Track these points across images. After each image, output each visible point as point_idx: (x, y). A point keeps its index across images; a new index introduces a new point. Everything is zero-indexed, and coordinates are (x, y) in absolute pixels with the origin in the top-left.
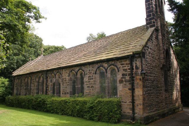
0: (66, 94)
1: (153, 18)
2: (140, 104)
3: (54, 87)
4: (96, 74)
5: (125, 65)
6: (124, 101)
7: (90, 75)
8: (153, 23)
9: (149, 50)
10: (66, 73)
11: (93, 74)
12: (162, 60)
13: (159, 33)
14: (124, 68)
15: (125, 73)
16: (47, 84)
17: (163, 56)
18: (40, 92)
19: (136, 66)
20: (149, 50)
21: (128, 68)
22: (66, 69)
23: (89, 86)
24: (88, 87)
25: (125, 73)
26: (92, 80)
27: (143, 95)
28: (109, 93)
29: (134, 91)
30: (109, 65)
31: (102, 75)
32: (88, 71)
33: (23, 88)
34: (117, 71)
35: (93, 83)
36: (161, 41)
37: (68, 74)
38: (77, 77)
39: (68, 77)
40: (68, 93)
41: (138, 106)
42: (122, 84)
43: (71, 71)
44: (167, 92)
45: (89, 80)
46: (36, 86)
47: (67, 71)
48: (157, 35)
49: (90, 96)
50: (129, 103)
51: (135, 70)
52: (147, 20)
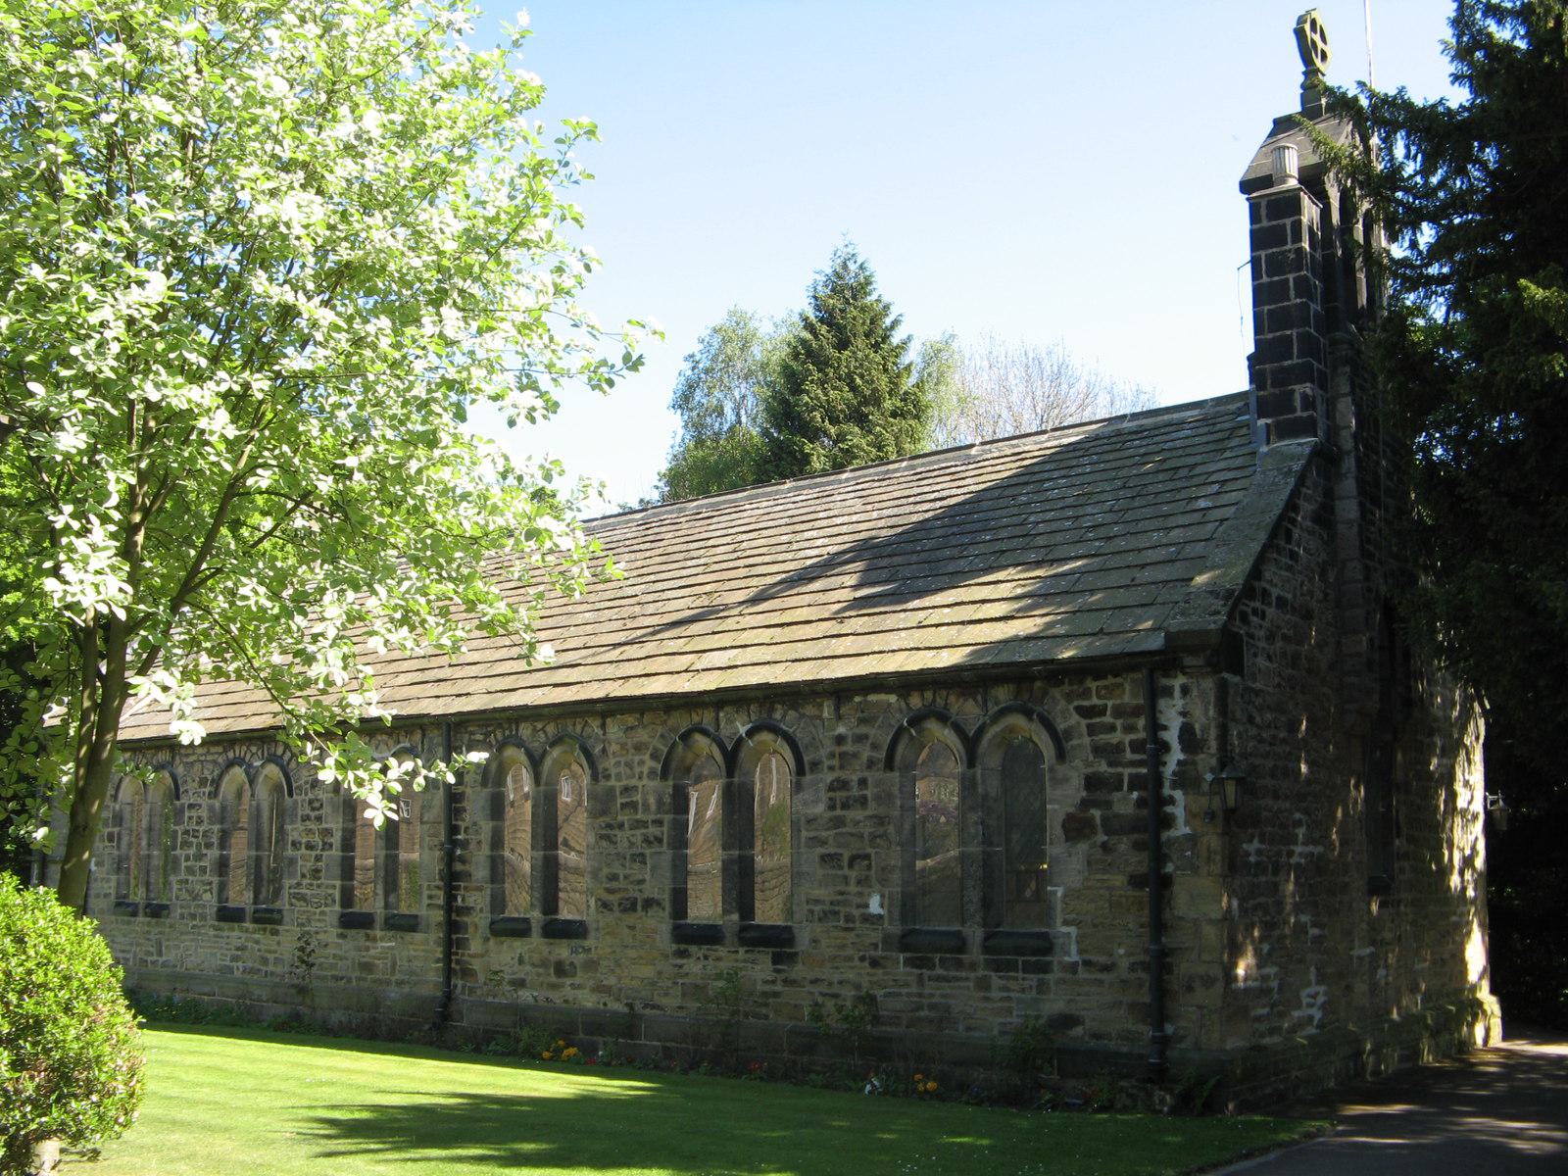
0: (633, 908)
1: (1304, 374)
5: (1108, 719)
7: (843, 775)
8: (1305, 408)
9: (1271, 612)
10: (639, 748)
14: (1104, 738)
15: (1110, 770)
19: (1187, 735)
20: (1271, 612)
21: (1133, 736)
23: (832, 851)
24: (825, 859)
25: (1110, 770)
26: (855, 814)
30: (993, 709)
32: (829, 746)
36: (1348, 534)
37: (654, 757)
39: (653, 784)
40: (648, 903)
42: (1082, 847)
43: (685, 737)
45: (832, 807)
47: (642, 735)
48: (1329, 495)
50: (1133, 976)
51: (1176, 755)
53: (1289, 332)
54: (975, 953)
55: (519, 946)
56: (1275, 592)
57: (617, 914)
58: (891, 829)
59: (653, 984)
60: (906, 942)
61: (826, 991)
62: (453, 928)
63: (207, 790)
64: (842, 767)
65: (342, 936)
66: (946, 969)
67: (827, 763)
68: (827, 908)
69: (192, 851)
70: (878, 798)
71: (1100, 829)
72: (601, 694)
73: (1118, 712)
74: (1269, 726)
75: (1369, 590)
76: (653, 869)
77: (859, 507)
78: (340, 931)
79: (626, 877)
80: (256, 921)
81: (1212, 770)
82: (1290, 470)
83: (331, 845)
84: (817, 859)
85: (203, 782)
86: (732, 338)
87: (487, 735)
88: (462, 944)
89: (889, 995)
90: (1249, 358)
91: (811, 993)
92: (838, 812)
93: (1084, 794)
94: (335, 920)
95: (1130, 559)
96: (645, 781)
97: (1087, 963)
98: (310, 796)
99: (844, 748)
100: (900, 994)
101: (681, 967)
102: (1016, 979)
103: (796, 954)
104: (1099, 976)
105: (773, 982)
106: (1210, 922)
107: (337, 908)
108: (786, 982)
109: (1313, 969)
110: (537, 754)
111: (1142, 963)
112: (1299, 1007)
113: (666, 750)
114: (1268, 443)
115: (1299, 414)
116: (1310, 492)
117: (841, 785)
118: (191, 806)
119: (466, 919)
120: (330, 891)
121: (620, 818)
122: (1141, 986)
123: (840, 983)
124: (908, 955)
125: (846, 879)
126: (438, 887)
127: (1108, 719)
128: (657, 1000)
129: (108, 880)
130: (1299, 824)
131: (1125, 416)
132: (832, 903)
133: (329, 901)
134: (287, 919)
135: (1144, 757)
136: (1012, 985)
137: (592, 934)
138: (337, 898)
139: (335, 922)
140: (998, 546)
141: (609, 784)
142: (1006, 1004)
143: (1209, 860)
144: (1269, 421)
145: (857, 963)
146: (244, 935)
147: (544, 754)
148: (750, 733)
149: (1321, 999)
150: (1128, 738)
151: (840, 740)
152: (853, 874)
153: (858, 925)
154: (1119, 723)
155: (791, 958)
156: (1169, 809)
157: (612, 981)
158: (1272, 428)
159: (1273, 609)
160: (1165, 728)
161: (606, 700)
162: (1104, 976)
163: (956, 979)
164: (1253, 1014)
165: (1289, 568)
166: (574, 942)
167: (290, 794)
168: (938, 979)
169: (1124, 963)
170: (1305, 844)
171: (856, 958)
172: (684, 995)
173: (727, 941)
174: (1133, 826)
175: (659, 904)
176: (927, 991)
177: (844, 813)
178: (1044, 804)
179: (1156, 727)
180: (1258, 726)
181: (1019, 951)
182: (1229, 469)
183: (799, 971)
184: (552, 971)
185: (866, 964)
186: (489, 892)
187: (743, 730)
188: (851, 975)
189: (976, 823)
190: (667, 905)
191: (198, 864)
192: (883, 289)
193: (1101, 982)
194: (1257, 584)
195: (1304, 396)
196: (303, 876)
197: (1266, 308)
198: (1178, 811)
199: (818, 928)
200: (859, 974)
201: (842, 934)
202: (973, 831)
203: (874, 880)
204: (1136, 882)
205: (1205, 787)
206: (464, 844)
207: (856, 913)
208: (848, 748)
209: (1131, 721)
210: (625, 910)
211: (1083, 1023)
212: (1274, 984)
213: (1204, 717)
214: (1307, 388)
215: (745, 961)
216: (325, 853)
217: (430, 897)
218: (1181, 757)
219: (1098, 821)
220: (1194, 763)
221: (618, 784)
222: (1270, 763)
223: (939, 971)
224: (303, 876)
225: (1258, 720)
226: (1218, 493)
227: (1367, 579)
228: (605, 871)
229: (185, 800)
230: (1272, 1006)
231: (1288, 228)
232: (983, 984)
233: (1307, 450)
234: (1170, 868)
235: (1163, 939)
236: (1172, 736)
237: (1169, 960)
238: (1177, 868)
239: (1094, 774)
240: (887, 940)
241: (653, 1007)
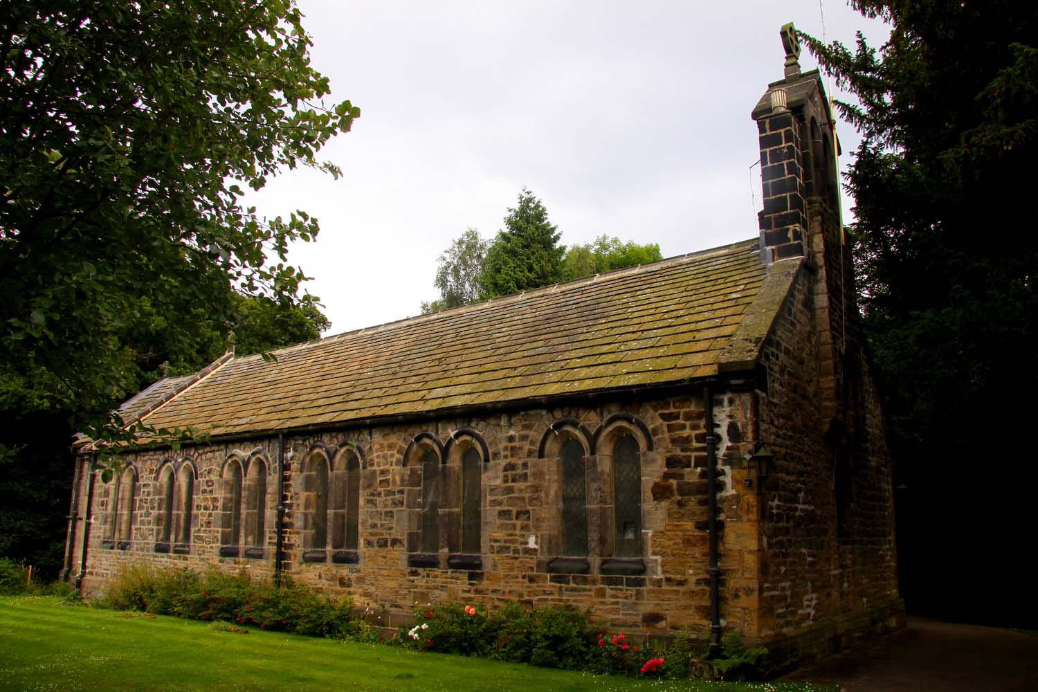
0: (386, 545)
1: (795, 219)
2: (749, 591)
3: (326, 514)
4: (541, 454)
5: (681, 421)
6: (673, 577)
9: (782, 355)
10: (390, 447)
11: (530, 454)
12: (829, 399)
13: (817, 281)
15: (683, 454)
16: (285, 498)
17: (832, 385)
18: (242, 534)
19: (732, 429)
20: (782, 355)
21: (697, 432)
22: (387, 430)
23: (506, 508)
24: (503, 514)
25: (683, 454)
26: (520, 485)
27: (760, 550)
28: (602, 541)
29: (720, 533)
31: (574, 467)
33: (148, 514)
34: (643, 444)
35: (527, 496)
36: (823, 316)
37: (399, 452)
38: (444, 468)
39: (397, 468)
40: (395, 542)
41: (737, 596)
42: (664, 504)
44: (845, 543)
45: (506, 481)
46: (220, 504)
49: (511, 554)
51: (726, 443)
52: (763, 219)
53: (784, 195)
54: (596, 573)
55: (319, 568)
56: (784, 344)
57: (377, 548)
58: (543, 494)
59: (397, 592)
60: (550, 567)
61: (500, 597)
62: (281, 557)
63: (153, 476)
64: (512, 456)
65: (222, 561)
66: (577, 584)
67: (503, 453)
68: (502, 544)
69: (143, 512)
70: (534, 475)
71: (676, 492)
72: (369, 414)
73: (688, 417)
74: (782, 427)
75: (836, 349)
76: (397, 521)
77: (529, 311)
78: (220, 558)
79: (382, 526)
80: (176, 552)
81: (750, 452)
82: (789, 273)
83: (217, 508)
84: (496, 514)
85: (151, 471)
86: (470, 245)
87: (304, 441)
88: (287, 566)
89: (540, 600)
90: (760, 214)
91: (492, 599)
92: (510, 484)
93: (666, 469)
94: (217, 551)
95: (692, 327)
96: (394, 467)
97: (668, 580)
98: (207, 478)
99: (513, 444)
100: (547, 600)
101: (413, 581)
102: (622, 590)
103: (483, 574)
104: (675, 588)
105: (469, 591)
106: (750, 552)
107: (219, 544)
108: (477, 591)
109: (809, 583)
110: (332, 452)
111: (705, 579)
112: (802, 607)
113: (406, 447)
114: (773, 260)
115: (792, 242)
116: (800, 287)
117: (510, 467)
118: (145, 485)
119: (289, 551)
120: (216, 534)
121: (379, 489)
122: (704, 594)
123: (510, 592)
124: (552, 574)
125: (514, 526)
126: (274, 532)
127: (681, 421)
128: (399, 602)
129: (100, 528)
130: (799, 490)
131: (684, 256)
132: (505, 542)
133: (215, 540)
134: (192, 551)
135: (705, 445)
136: (619, 594)
137: (361, 561)
138: (220, 538)
139: (218, 554)
140: (610, 325)
141: (374, 468)
142: (615, 606)
143: (748, 511)
144: (773, 247)
145: (520, 580)
146: (168, 560)
147: (336, 451)
148: (457, 436)
149: (814, 603)
150: (694, 433)
151: (511, 439)
152: (519, 523)
153: (521, 555)
154: (688, 423)
155: (480, 576)
156: (721, 478)
157: (372, 589)
158: (776, 253)
159: (782, 355)
160: (718, 426)
161: (373, 417)
162: (680, 588)
163: (585, 590)
164: (776, 612)
165: (791, 331)
166: (352, 566)
167: (197, 478)
168: (573, 590)
169: (693, 579)
170: (803, 503)
171: (520, 576)
172: (415, 599)
173: (441, 566)
174: (699, 489)
175: (401, 543)
176: (565, 598)
177: (513, 484)
178: (639, 478)
179: (712, 425)
180: (776, 427)
181: (624, 571)
182: (750, 277)
183: (485, 584)
184: (338, 583)
185: (526, 580)
186: (302, 535)
187: (452, 434)
188: (517, 587)
189: (596, 490)
190: (405, 542)
191: (147, 519)
192: (552, 219)
193: (677, 592)
194: (773, 337)
195: (795, 232)
196: (202, 526)
197: (770, 181)
198: (728, 479)
199: (496, 557)
200: (519, 586)
201: (511, 561)
202: (594, 494)
203: (531, 527)
204: (700, 526)
205: (745, 464)
206: (290, 506)
207: (520, 547)
208: (516, 444)
209: (696, 422)
210: (380, 546)
211: (665, 619)
212: (788, 593)
213: (744, 418)
214: (798, 227)
215: (452, 578)
216: (214, 512)
217: (270, 538)
218: (730, 444)
219: (675, 487)
220: (738, 448)
221: (378, 468)
222: (783, 451)
223: (572, 585)
224: (202, 526)
225: (776, 422)
226: (743, 290)
227: (834, 343)
228: (370, 521)
229: (141, 482)
230: (787, 607)
231: (783, 135)
232: (601, 594)
233: (798, 262)
234: (722, 517)
235: (719, 564)
236: (723, 431)
237: (723, 577)
238: (727, 517)
239: (672, 456)
240: (539, 564)
241: (396, 606)
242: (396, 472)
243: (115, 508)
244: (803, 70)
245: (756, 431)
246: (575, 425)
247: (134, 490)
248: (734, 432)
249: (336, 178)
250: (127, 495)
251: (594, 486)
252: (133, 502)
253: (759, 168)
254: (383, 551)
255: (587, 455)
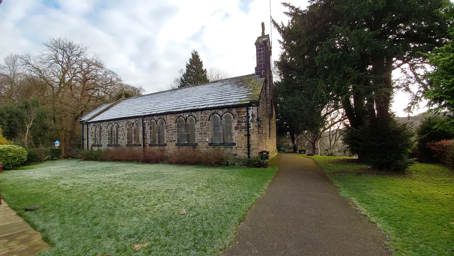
19: (252, 115)
26: (205, 127)
33: (105, 138)
42: (237, 131)
46: (126, 134)
51: (251, 118)
52: (256, 69)
151: (202, 117)
152: (204, 136)
179: (248, 114)
242: (174, 125)
243: (95, 136)
244: (265, 34)
245: (258, 115)
246: (217, 113)
247: (100, 132)
248: (253, 115)
249: (309, 2)
250: (99, 133)
251: (221, 127)
252: (100, 134)
253: (256, 57)
254: (171, 143)
255: (220, 120)
